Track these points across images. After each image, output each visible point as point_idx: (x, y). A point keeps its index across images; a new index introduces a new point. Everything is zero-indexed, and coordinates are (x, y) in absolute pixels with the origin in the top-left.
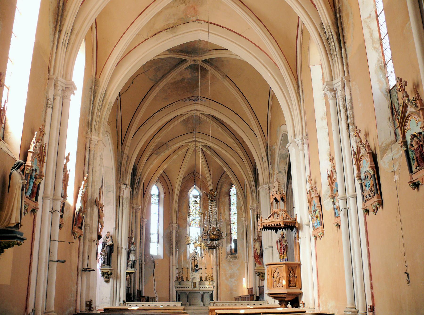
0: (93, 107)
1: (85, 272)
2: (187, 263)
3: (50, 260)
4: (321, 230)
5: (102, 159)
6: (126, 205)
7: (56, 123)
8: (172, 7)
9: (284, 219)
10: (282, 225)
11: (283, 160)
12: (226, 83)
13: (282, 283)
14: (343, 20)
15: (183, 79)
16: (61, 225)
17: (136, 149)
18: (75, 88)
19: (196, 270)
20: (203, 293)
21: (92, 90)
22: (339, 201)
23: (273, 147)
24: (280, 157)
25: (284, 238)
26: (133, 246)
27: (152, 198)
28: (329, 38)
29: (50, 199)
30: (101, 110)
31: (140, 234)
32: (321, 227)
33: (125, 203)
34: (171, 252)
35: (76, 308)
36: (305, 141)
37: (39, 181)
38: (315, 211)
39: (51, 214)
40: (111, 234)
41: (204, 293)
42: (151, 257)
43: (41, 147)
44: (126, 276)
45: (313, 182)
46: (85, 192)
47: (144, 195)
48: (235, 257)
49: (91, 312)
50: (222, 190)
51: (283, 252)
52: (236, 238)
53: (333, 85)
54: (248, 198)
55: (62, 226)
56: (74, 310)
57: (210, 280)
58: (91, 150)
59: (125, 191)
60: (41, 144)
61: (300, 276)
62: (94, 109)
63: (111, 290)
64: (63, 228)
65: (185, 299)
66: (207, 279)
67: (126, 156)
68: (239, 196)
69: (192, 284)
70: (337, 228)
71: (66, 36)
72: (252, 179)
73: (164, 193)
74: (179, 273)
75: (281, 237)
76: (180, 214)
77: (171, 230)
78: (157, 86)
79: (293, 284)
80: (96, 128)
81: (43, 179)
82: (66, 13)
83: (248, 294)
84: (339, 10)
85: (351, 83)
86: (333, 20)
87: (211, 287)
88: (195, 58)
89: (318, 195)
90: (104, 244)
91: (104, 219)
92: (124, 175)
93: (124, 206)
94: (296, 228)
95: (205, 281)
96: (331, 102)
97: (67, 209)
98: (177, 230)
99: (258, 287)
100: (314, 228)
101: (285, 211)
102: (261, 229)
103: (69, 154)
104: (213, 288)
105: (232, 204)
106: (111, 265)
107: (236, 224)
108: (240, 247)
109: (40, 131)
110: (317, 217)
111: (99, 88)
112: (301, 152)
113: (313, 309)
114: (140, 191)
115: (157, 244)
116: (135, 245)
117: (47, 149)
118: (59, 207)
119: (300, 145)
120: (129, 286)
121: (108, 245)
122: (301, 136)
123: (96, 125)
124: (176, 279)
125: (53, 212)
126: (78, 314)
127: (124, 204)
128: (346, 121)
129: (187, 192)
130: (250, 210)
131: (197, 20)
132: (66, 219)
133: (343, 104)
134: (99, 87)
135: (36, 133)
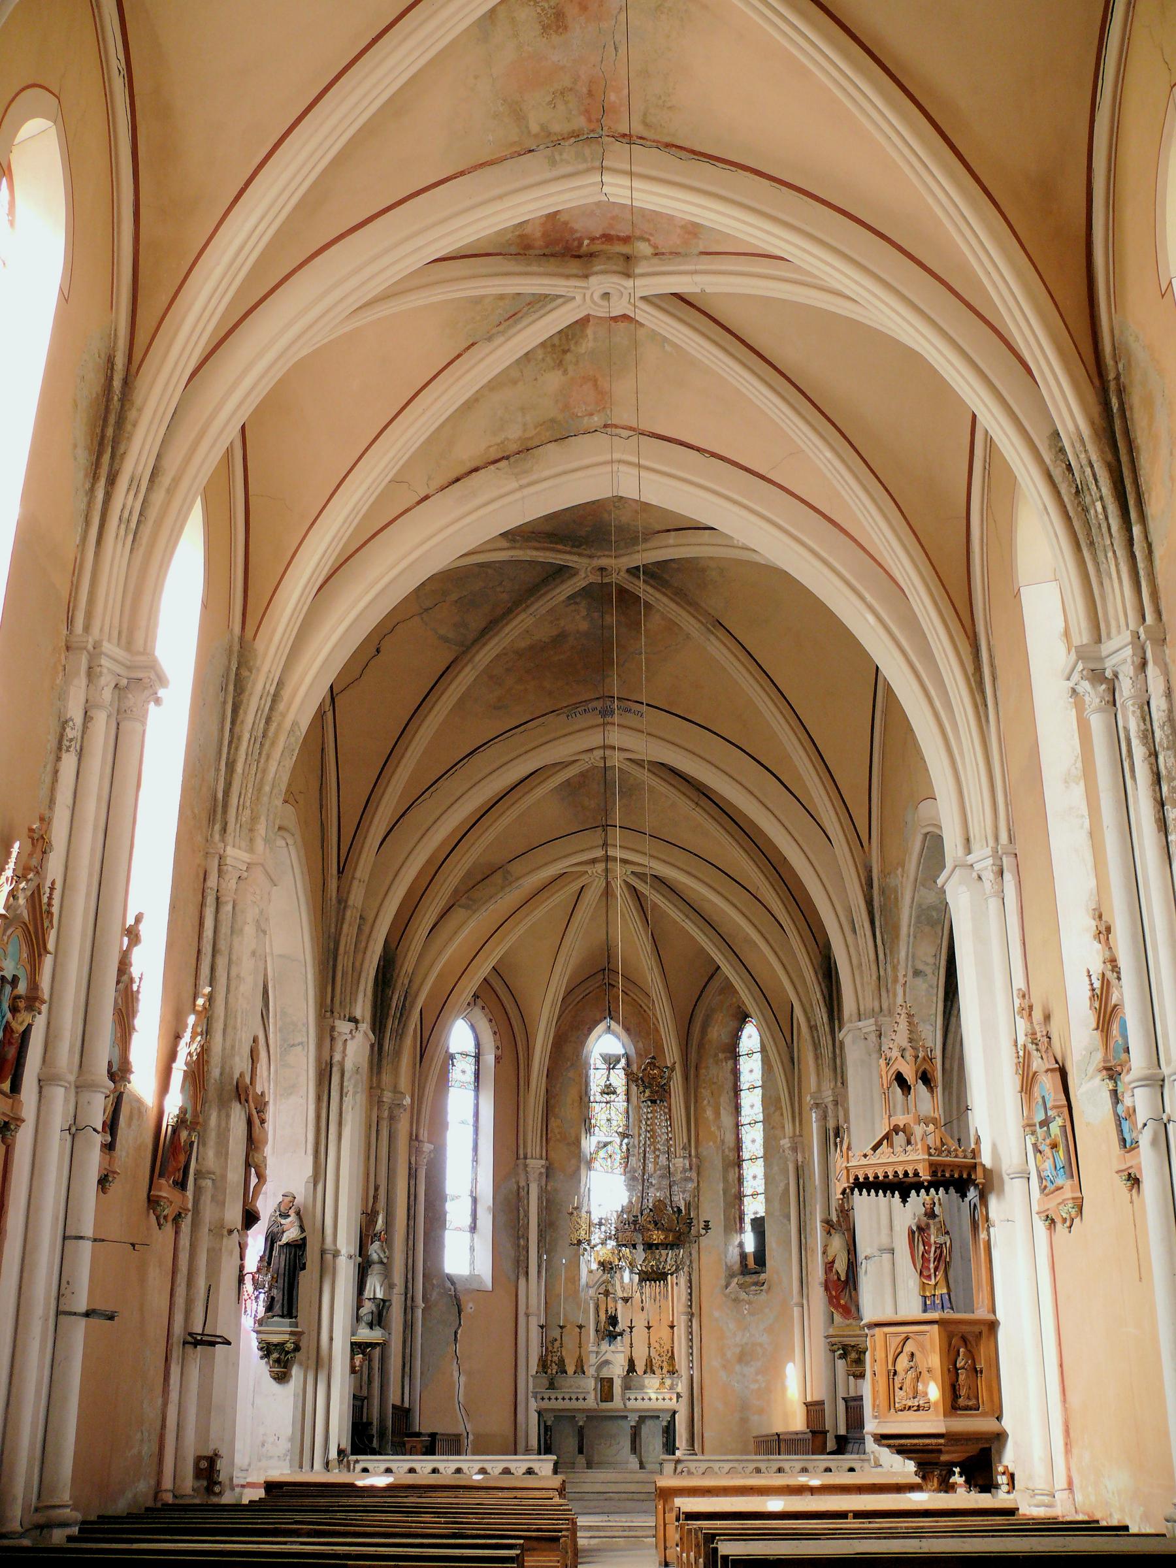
0: (230, 743)
1: (196, 1347)
2: (579, 1306)
3: (61, 1308)
4: (1069, 1195)
5: (264, 932)
6: (355, 1093)
7: (91, 808)
8: (515, 382)
9: (930, 1155)
10: (925, 1176)
11: (927, 929)
12: (717, 649)
13: (926, 1394)
14: (1132, 419)
15: (558, 636)
16: (106, 1176)
17: (390, 894)
18: (162, 680)
19: (612, 1337)
20: (638, 1422)
21: (227, 680)
22: (1135, 1090)
23: (892, 881)
24: (918, 917)
25: (937, 1220)
26: (376, 1245)
27: (453, 1065)
28: (1085, 488)
29: (66, 1084)
30: (260, 754)
31: (409, 1197)
32: (1071, 1186)
33: (349, 1085)
34: (520, 1265)
35: (159, 1483)
36: (1007, 862)
37: (25, 1017)
38: (1045, 1123)
39: (69, 1138)
40: (300, 1200)
41: (642, 1419)
42: (448, 1284)
43: (35, 898)
44: (352, 1359)
45: (1037, 1015)
46: (198, 1055)
47: (422, 1056)
48: (756, 1284)
49: (215, 1500)
50: (709, 1036)
51: (932, 1271)
52: (762, 1213)
53: (1101, 659)
54: (801, 1066)
55: (110, 1179)
56: (152, 1493)
57: (665, 1371)
58: (222, 899)
59: (349, 1042)
60: (33, 885)
61: (994, 1370)
62: (237, 749)
63: (295, 1408)
64: (115, 1187)
65: (571, 1443)
66: (654, 1368)
67: (356, 918)
68: (772, 1058)
69: (596, 1384)
70: (1131, 1190)
71: (132, 493)
72: (816, 994)
73: (498, 1048)
74: (549, 1345)
75: (926, 1214)
76: (553, 1123)
77: (522, 1184)
78: (466, 665)
79: (969, 1398)
80: (244, 819)
81: (39, 1013)
82: (132, 415)
83: (808, 1427)
84: (1118, 384)
85: (1167, 652)
86: (1097, 420)
87: (667, 1396)
88: (604, 562)
89: (1057, 1062)
90: (272, 1239)
91: (268, 1150)
92: (349, 985)
93: (348, 1100)
94: (976, 1186)
95: (645, 1373)
96: (1097, 723)
97: (131, 1118)
98: (543, 1183)
99: (843, 1398)
100: (1046, 1187)
101: (934, 1121)
102: (848, 1190)
103: (138, 919)
104: (675, 1400)
105: (743, 1087)
106: (296, 1317)
107: (761, 1162)
108: (774, 1245)
109: (33, 839)
110: (1054, 1146)
111: (253, 676)
112: (993, 904)
113: (1046, 1499)
114: (408, 1041)
115: (468, 1234)
116: (388, 1242)
117: (56, 902)
118: (97, 1116)
119: (989, 876)
120: (364, 1393)
121: (287, 1244)
122: (991, 842)
123: (241, 808)
124: (538, 1366)
125: (75, 1130)
126: (167, 1507)
127: (345, 1090)
128: (1154, 790)
129: (582, 1042)
130: (811, 1109)
131: (605, 426)
132: (128, 1153)
133: (1142, 727)
134: (254, 671)
135: (17, 845)
